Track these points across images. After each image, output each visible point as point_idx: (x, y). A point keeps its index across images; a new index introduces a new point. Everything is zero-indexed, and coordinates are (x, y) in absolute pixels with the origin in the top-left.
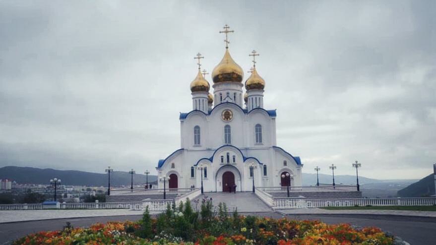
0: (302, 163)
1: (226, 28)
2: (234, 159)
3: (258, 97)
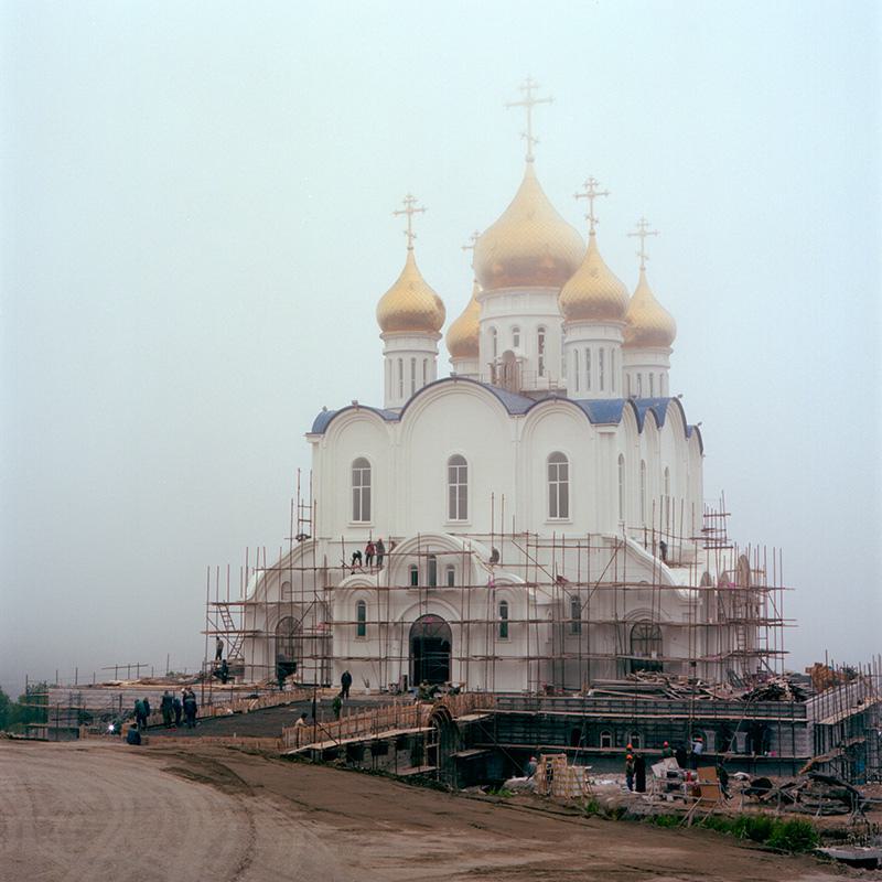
3: (420, 359)
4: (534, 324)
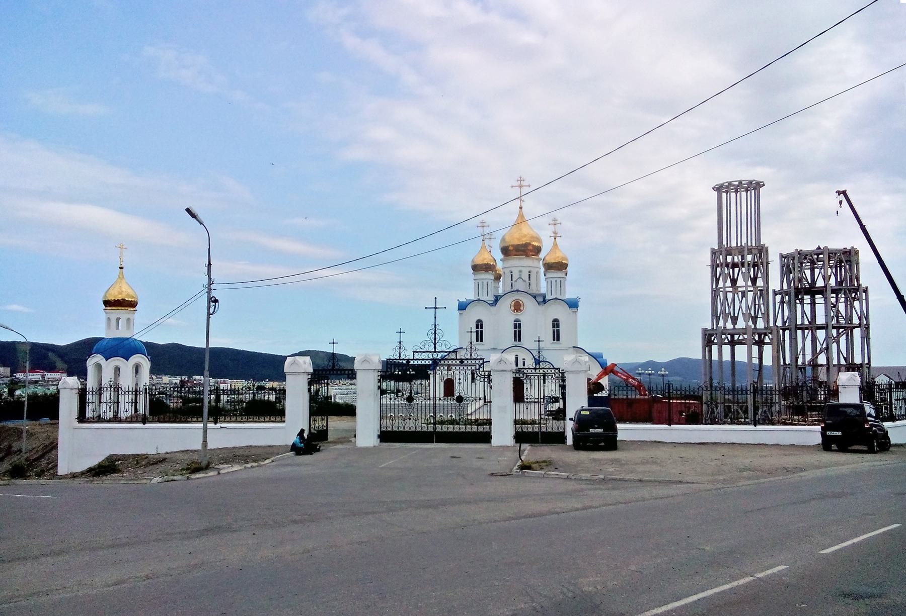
4: (527, 270)
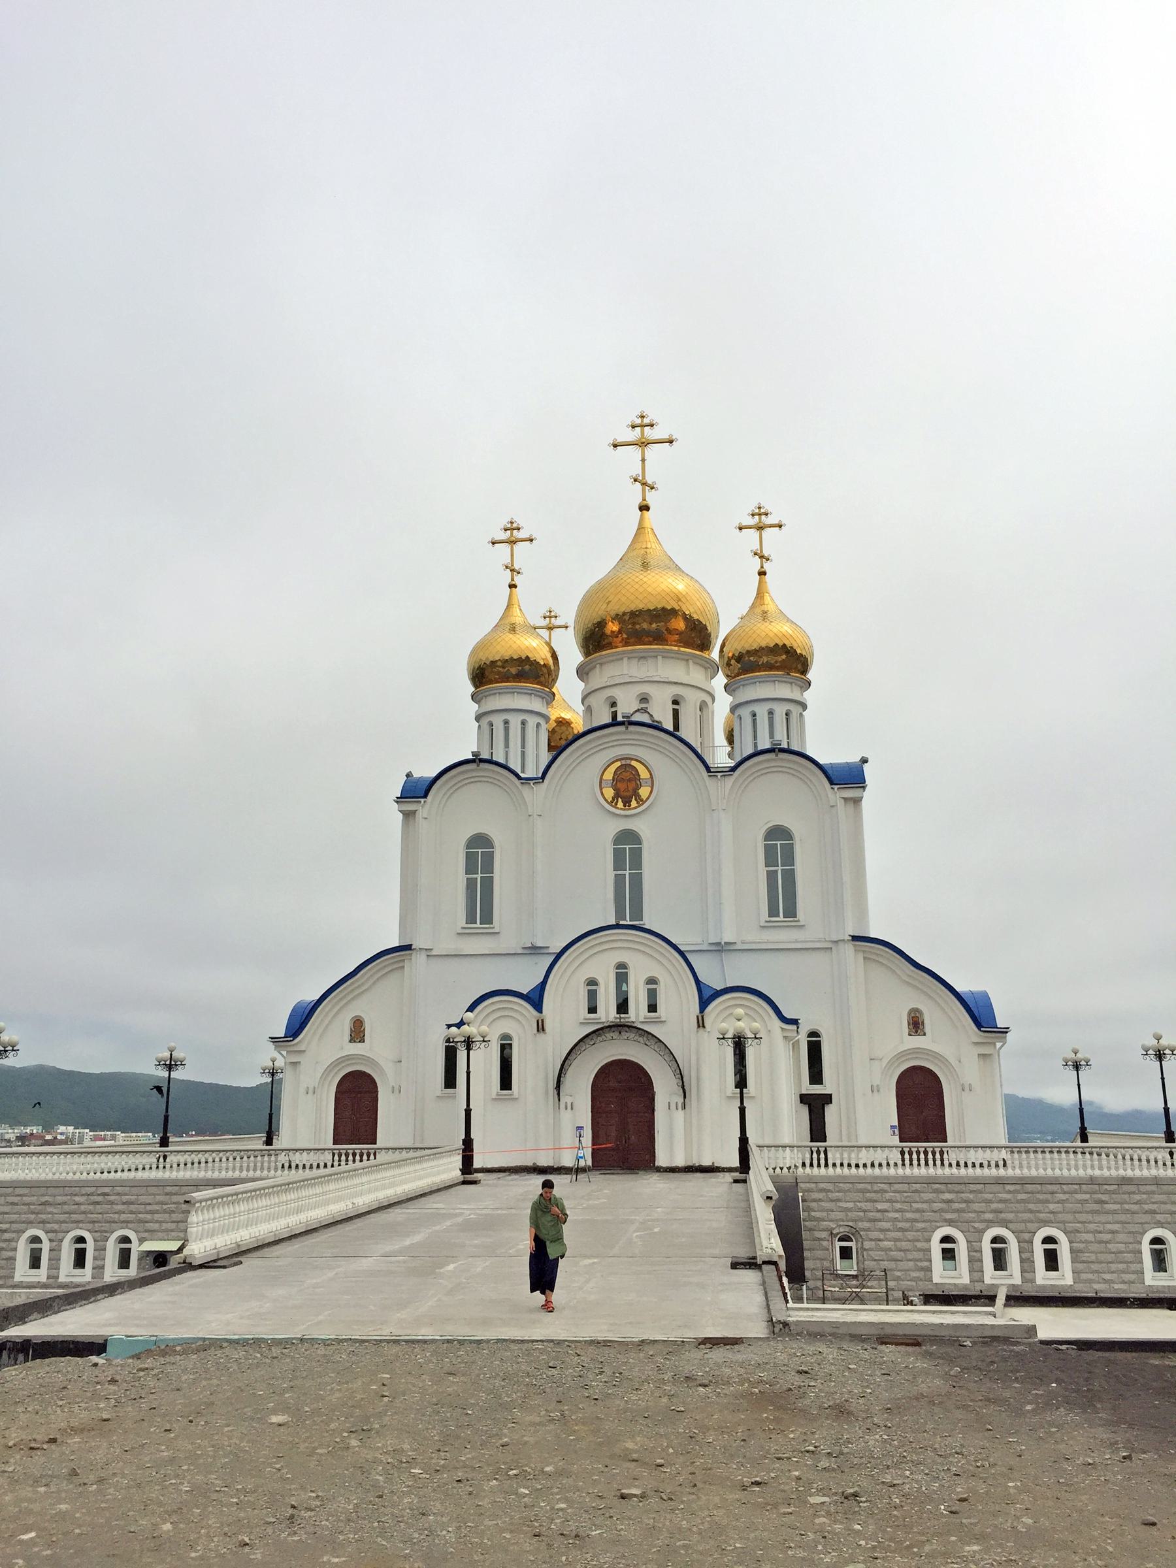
0: (1000, 1023)
1: (642, 426)
2: (652, 995)
3: (780, 710)
